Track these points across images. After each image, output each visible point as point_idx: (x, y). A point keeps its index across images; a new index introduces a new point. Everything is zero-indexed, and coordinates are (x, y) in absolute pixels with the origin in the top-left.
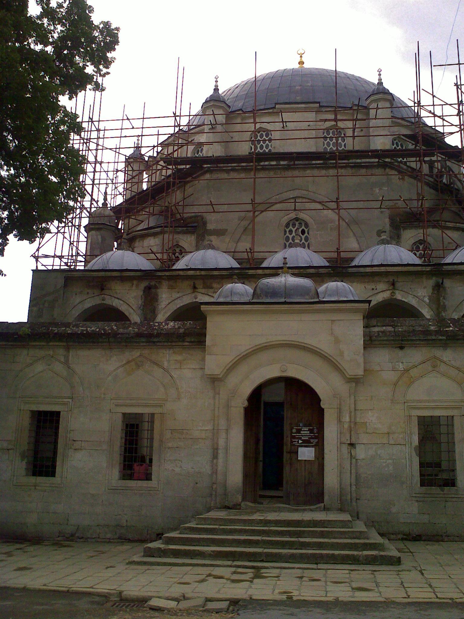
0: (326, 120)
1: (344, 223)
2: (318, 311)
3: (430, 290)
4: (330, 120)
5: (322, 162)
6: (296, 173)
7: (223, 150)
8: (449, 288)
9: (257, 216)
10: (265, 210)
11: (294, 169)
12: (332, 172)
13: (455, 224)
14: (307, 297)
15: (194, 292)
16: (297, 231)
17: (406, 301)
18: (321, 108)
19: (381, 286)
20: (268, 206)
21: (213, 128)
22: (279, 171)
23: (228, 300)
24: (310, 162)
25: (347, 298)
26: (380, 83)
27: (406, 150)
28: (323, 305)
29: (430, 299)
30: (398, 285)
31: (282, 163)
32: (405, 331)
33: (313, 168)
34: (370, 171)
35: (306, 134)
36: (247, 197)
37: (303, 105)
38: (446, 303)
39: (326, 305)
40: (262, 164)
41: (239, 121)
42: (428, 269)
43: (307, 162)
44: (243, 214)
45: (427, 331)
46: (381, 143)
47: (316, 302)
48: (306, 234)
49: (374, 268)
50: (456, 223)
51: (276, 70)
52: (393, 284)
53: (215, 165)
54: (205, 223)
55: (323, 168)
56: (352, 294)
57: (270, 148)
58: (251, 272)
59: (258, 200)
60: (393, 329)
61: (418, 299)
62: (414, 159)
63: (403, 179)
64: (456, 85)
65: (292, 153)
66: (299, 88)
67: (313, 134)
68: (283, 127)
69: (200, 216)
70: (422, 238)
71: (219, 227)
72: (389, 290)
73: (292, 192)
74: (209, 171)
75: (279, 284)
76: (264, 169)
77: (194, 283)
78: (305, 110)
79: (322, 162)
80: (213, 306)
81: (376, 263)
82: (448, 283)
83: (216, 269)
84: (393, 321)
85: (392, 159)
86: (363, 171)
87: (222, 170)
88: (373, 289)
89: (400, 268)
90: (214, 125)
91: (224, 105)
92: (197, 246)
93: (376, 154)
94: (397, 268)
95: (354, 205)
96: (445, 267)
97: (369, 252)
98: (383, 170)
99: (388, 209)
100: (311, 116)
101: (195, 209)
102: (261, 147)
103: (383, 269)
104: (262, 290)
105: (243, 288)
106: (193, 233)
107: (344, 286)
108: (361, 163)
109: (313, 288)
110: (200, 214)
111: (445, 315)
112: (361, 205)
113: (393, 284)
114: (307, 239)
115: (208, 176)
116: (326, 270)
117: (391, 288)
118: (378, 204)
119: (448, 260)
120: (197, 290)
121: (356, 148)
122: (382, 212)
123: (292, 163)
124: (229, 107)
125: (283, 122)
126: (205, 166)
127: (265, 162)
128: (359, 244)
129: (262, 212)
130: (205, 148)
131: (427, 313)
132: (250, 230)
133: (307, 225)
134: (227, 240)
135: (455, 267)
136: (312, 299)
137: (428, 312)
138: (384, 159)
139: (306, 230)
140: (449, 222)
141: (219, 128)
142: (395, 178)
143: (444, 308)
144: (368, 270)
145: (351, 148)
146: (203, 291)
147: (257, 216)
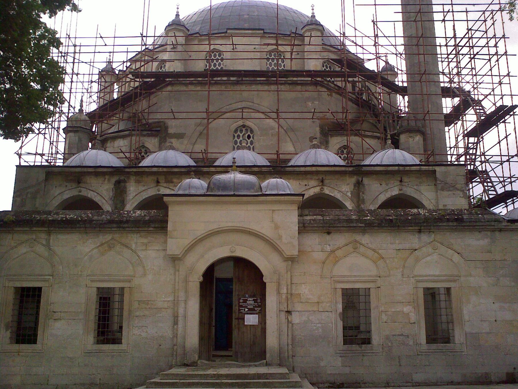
0: (268, 45)
1: (283, 130)
3: (353, 187)
4: (272, 44)
6: (243, 87)
10: (218, 118)
11: (242, 84)
12: (273, 87)
14: (252, 191)
15: (157, 186)
16: (244, 136)
17: (332, 195)
18: (265, 34)
19: (313, 183)
20: (220, 114)
21: (174, 48)
23: (187, 192)
24: (256, 79)
25: (284, 191)
26: (313, 16)
28: (265, 198)
29: (351, 194)
30: (326, 182)
31: (232, 79)
32: (332, 220)
34: (304, 88)
35: (252, 55)
36: (202, 107)
39: (268, 197)
40: (215, 79)
41: (196, 43)
43: (253, 79)
46: (314, 65)
47: (259, 195)
48: (251, 139)
49: (307, 168)
54: (166, 128)
57: (222, 66)
60: (322, 218)
62: (340, 79)
63: (331, 95)
64: (373, 21)
65: (240, 71)
66: (247, 16)
67: (258, 55)
70: (346, 144)
71: (179, 131)
74: (171, 84)
75: (229, 179)
76: (216, 83)
77: (157, 178)
80: (174, 198)
82: (366, 181)
84: (322, 211)
85: (322, 78)
86: (299, 88)
87: (181, 84)
88: (306, 185)
89: (328, 168)
94: (326, 168)
96: (364, 168)
97: (303, 154)
98: (315, 87)
100: (257, 40)
101: (158, 116)
103: (314, 169)
104: (214, 184)
109: (257, 184)
112: (297, 115)
113: (322, 181)
114: (252, 143)
115: (169, 88)
119: (367, 162)
123: (240, 79)
126: (167, 79)
129: (215, 119)
130: (168, 64)
131: (349, 205)
132: (205, 134)
133: (252, 131)
134: (186, 142)
135: (372, 168)
137: (350, 204)
139: (251, 135)
141: (179, 48)
142: (325, 94)
143: (363, 201)
144: (302, 169)
146: (165, 185)
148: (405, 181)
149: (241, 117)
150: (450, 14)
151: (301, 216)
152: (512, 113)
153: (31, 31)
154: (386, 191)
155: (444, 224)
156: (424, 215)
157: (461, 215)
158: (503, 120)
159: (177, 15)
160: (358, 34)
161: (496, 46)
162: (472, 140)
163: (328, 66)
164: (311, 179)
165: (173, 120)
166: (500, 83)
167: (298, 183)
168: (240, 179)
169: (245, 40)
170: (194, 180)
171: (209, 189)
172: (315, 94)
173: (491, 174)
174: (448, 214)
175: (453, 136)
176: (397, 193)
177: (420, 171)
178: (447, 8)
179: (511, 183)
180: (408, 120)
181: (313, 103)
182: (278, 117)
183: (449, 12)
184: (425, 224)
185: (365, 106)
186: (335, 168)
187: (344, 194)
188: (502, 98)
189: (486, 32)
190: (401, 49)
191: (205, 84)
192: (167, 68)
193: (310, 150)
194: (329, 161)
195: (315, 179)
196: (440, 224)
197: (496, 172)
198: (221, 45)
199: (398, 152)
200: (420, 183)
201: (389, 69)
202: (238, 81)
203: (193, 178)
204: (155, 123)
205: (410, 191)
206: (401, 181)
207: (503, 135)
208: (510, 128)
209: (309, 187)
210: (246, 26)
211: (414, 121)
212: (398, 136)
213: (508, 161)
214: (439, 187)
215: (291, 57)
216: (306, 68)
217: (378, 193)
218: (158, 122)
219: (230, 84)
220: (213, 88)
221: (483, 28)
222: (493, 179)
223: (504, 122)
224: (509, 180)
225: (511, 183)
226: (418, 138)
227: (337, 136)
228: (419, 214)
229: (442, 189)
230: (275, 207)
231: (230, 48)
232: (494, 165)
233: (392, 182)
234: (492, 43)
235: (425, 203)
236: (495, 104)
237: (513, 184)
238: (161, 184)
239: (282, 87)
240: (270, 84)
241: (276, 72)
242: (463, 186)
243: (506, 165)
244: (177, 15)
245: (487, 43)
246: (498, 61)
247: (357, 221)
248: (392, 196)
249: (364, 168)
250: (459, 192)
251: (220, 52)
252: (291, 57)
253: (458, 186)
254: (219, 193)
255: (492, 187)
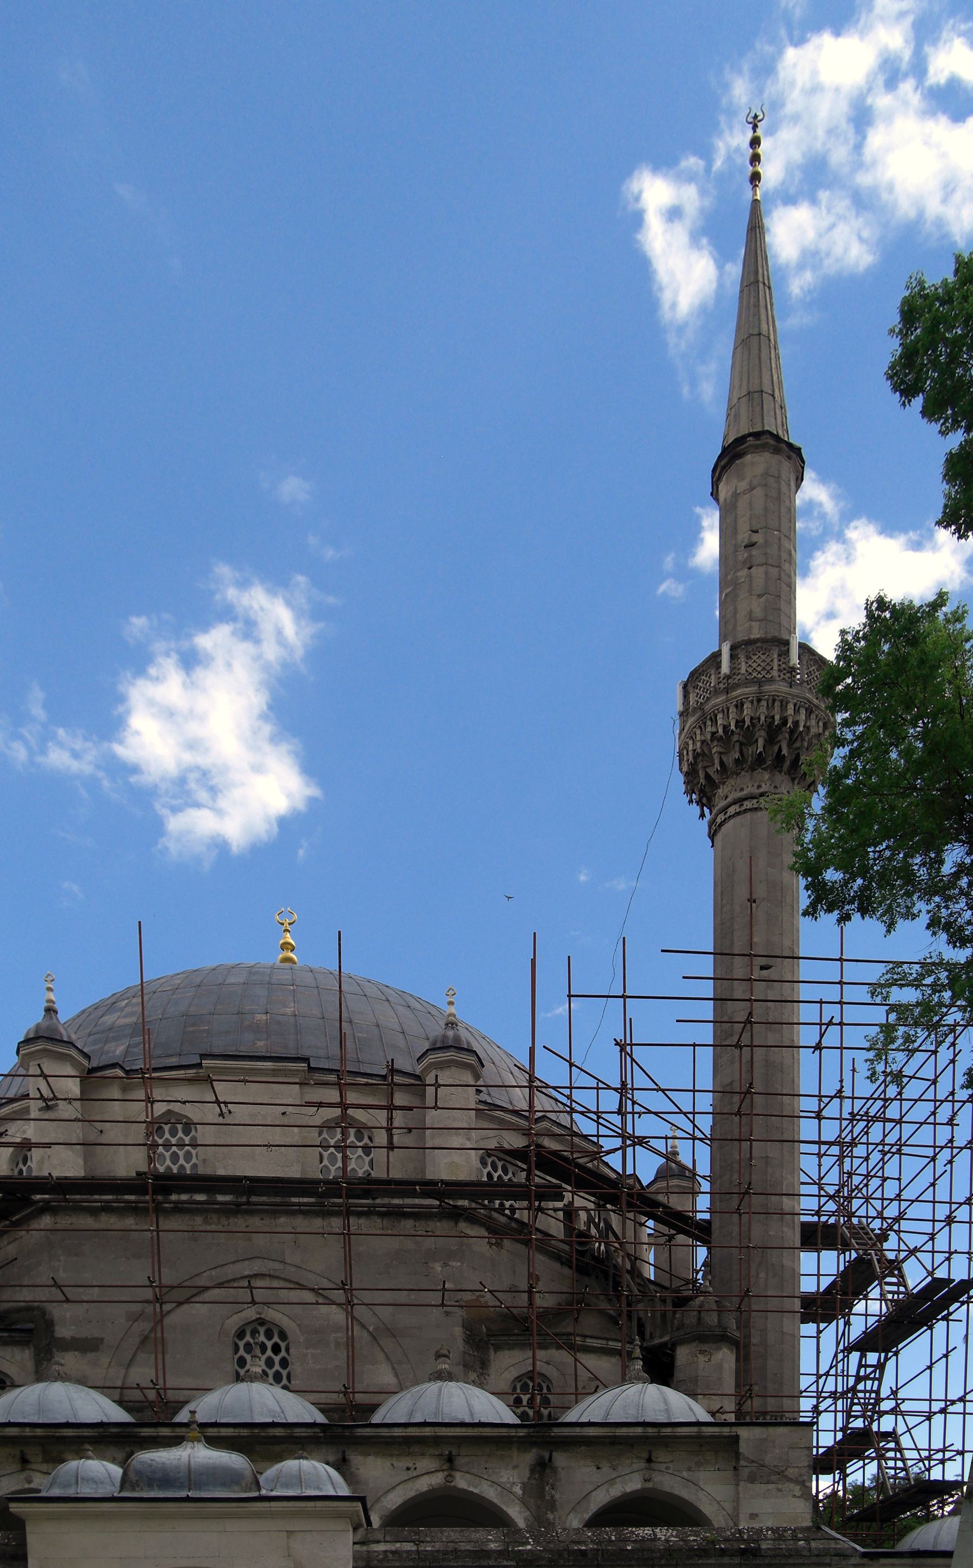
0: (320, 1105)
1: (365, 1334)
2: (272, 1515)
3: (527, 1473)
4: (330, 1105)
5: (312, 1200)
6: (255, 1222)
7: (81, 1162)
8: (563, 1469)
9: (169, 1312)
10: (187, 1301)
11: (251, 1213)
12: (336, 1223)
13: (605, 1342)
14: (236, 1488)
15: (23, 1470)
16: (261, 1347)
17: (476, 1491)
18: (310, 1072)
19: (425, 1464)
20: (191, 1293)
21: (48, 1108)
22: (215, 1217)
23: (71, 1492)
24: (287, 1199)
25: (319, 1489)
27: (510, 1184)
28: (267, 1504)
29: (524, 1488)
30: (460, 1461)
31: (220, 1198)
32: (438, 1551)
33: (294, 1213)
34: (421, 1227)
35: (276, 1136)
36: (140, 1271)
37: (269, 1065)
38: (557, 1496)
39: (273, 1504)
40: (174, 1197)
41: (117, 1094)
42: (522, 1432)
43: (278, 1200)
44: (136, 1308)
45: (482, 1551)
46: (456, 1162)
47: (252, 1502)
48: (283, 1353)
49: (410, 1429)
50: (608, 1340)
51: (215, 964)
52: (450, 1460)
53: (61, 1197)
54: (50, 1325)
55: (317, 1214)
56: (333, 1484)
57: (194, 1160)
58: (146, 1432)
59: (169, 1277)
60: (414, 1548)
61: (499, 1489)
63: (499, 1245)
65: (238, 1179)
66: (264, 1017)
67: (295, 1136)
68: (222, 1114)
69: (38, 1308)
71: (85, 1333)
72: (443, 1471)
73: (247, 1263)
74: (46, 1208)
75: (175, 1462)
76: (178, 1209)
77: (22, 1452)
78: (275, 1078)
79: (312, 1200)
80: (36, 1505)
81: (418, 1419)
82: (561, 1459)
83: (68, 1425)
84: (418, 1533)
85: (472, 1200)
86: (408, 1224)
87: (78, 1209)
88: (408, 1469)
89: (464, 1430)
90: (51, 1100)
91: (73, 1053)
92: (37, 1372)
93: (431, 1188)
94: (458, 1430)
95: (388, 1297)
96: (556, 1430)
97: (409, 1395)
98: (452, 1224)
99: (462, 1307)
100: (291, 1093)
101: (26, 1295)
102: (175, 1158)
103: (427, 1431)
104: (139, 1473)
105: (102, 1469)
106: (24, 1344)
107: (315, 1467)
108: (402, 1206)
109: (248, 1473)
110: (36, 1304)
111: (554, 1519)
112: (402, 1297)
113: (450, 1460)
114: (284, 1363)
115: (46, 1221)
116: (309, 1430)
117: (445, 1467)
118: (436, 1298)
119: (572, 1416)
120: (29, 1466)
121: (396, 1174)
122: (447, 1314)
123: (244, 1199)
124: (87, 1056)
125: (218, 1102)
126: (38, 1197)
127: (179, 1194)
128: (396, 1375)
129: (180, 1304)
130: (36, 1154)
131: (517, 1514)
132: (154, 1343)
133: (283, 1335)
134: (105, 1360)
135: (578, 1430)
136: (245, 1492)
137: (520, 1512)
138: (450, 1202)
139: (283, 1345)
140: (592, 1337)
141: (65, 1110)
143: (552, 1506)
144: (398, 1432)
145: (383, 1175)
146: (44, 1467)
147: (169, 1312)
148: (660, 1460)
149: (249, 1300)
150: (834, 1030)
151: (362, 1543)
152: (964, 1298)
153: (293, 489)
154: (611, 1482)
155: (709, 1561)
156: (667, 1541)
157: (754, 1541)
158: (946, 1312)
159: (50, 1011)
160: (581, 1079)
161: (951, 1122)
162: (872, 1358)
163: (500, 1164)
164: (423, 1455)
165: (65, 1305)
166: (950, 1220)
167: (388, 1464)
168: (205, 1461)
169: (255, 1092)
170: (90, 1462)
171: (127, 1485)
172: (453, 1244)
173: (905, 1441)
174: (726, 1540)
175: (817, 1351)
176: (639, 1486)
177: (699, 1437)
178: (831, 1012)
179: (942, 1462)
180: (699, 1312)
181: (446, 1265)
182: (349, 1304)
183: (830, 1023)
184: (663, 1562)
185: (595, 1268)
186: (481, 1429)
187: (506, 1490)
188: (948, 1259)
189: (934, 1082)
190: (705, 1123)
191: (145, 1211)
192: (33, 1164)
193: (427, 1385)
194: (472, 1415)
195: (432, 1455)
196: (700, 1562)
197: (917, 1437)
198: (184, 1103)
199: (653, 1390)
200: (699, 1464)
201: (674, 1171)
202: (238, 1205)
203: (88, 1458)
204: (19, 1310)
205: (671, 1482)
206: (649, 1460)
207: (939, 1350)
208: (957, 1330)
209: (415, 1474)
210: (261, 1046)
211: (715, 1314)
212: (673, 1349)
213: (943, 1411)
214: (745, 1473)
215: (158, 1235)
216: (429, 1176)
217: (591, 1488)
218: (28, 1309)
219: (216, 1211)
220: (165, 1224)
221: (928, 1072)
222: (908, 1454)
223: (946, 1318)
224: (939, 1456)
225: (942, 1462)
226: (726, 1358)
227: (511, 1347)
228: (655, 1539)
229: (752, 1479)
230: (294, 1525)
231: (211, 1113)
232: (912, 1421)
233: (628, 1462)
234: (944, 1112)
235: (708, 1509)
236: (930, 1273)
237: (948, 1464)
238: (34, 1466)
239: (362, 1221)
240: (326, 1213)
241: (338, 1183)
242: (804, 1471)
243: (938, 1419)
244: (50, 1011)
245: (934, 1113)
246: (950, 1162)
247: (500, 1553)
248: (625, 1495)
249: (556, 1431)
250: (792, 1486)
251: (189, 1126)
252: (158, 1235)
253: (791, 1472)
254: (152, 1494)
255: (902, 1469)
